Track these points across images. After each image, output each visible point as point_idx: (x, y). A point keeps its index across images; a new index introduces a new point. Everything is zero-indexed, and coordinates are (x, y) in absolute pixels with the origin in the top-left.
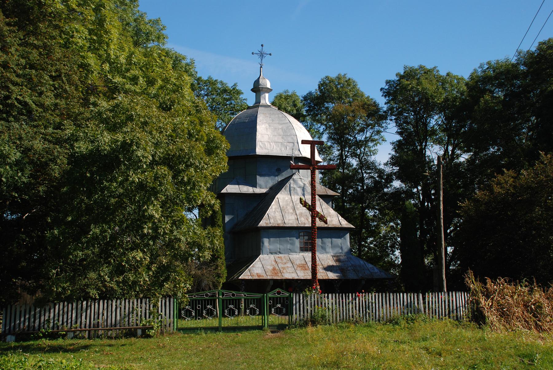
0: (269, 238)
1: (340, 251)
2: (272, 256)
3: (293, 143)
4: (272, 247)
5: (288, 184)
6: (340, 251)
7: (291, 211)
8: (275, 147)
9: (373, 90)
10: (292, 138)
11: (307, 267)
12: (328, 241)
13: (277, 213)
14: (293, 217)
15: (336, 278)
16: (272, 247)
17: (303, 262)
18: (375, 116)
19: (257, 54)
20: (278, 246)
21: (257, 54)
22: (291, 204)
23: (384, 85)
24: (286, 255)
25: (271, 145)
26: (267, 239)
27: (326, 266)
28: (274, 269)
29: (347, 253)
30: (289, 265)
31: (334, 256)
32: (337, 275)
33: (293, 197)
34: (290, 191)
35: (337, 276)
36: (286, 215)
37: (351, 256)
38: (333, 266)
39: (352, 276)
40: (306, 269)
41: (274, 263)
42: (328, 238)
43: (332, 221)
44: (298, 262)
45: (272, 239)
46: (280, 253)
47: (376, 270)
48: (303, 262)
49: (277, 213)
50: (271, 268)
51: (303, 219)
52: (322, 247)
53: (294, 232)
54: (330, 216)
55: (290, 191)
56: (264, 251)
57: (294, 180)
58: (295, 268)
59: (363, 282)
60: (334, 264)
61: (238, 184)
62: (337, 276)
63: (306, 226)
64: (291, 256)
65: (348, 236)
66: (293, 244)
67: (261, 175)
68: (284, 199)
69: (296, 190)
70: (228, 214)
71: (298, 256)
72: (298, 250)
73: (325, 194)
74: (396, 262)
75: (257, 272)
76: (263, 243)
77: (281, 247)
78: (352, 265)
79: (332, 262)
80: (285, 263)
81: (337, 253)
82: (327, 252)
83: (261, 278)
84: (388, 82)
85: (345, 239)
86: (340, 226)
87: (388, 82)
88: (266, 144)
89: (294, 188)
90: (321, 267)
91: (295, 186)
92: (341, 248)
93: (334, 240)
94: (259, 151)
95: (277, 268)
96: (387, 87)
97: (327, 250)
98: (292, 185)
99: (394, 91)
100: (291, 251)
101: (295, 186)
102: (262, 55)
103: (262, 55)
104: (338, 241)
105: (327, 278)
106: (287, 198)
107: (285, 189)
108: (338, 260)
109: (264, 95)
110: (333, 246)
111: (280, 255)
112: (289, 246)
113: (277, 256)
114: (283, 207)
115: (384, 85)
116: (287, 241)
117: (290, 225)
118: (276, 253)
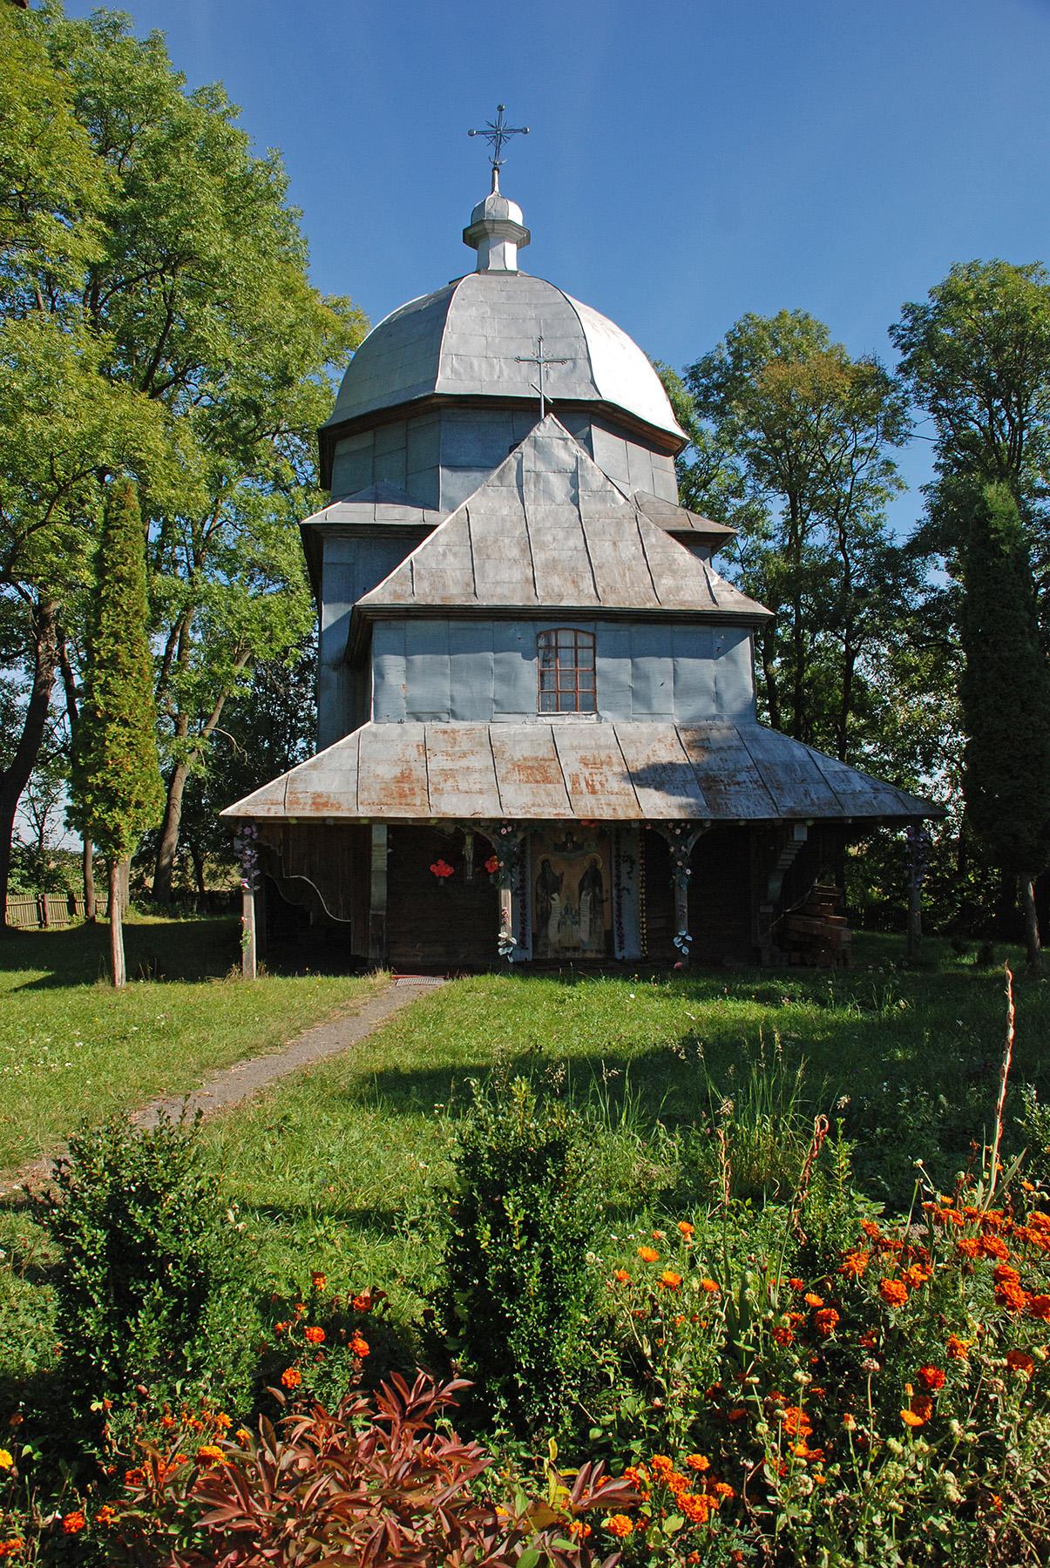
0: (406, 652)
1: (713, 710)
2: (415, 730)
3: (574, 360)
4: (417, 691)
5: (511, 460)
6: (713, 710)
7: (515, 552)
8: (506, 373)
9: (866, 336)
10: (571, 345)
11: (553, 772)
12: (659, 667)
13: (450, 558)
14: (518, 574)
15: (676, 815)
16: (417, 691)
17: (545, 751)
18: (870, 401)
19: (483, 133)
20: (446, 686)
21: (483, 133)
22: (519, 530)
23: (897, 318)
24: (478, 725)
25: (491, 366)
26: (400, 660)
27: (639, 764)
28: (404, 778)
29: (740, 716)
30: (481, 760)
31: (685, 730)
32: (684, 800)
33: (530, 508)
34: (520, 486)
35: (681, 807)
36: (489, 566)
37: (757, 729)
38: (671, 767)
39: (746, 807)
40: (547, 780)
41: (412, 753)
42: (659, 654)
43: (679, 589)
44: (521, 752)
45: (418, 659)
46: (453, 714)
47: (858, 784)
48: (545, 751)
49: (450, 558)
50: (388, 772)
51: (556, 581)
52: (635, 694)
53: (515, 630)
54: (674, 573)
55: (520, 486)
56: (385, 708)
57: (535, 444)
58: (502, 771)
59: (801, 835)
60: (679, 757)
61: (376, 499)
62: (681, 807)
63: (564, 603)
64: (496, 729)
65: (745, 648)
66: (508, 678)
67: (454, 467)
68: (493, 511)
69: (547, 482)
70: (333, 600)
71: (529, 728)
72: (532, 704)
73: (688, 528)
74: (934, 798)
75: (320, 789)
76: (381, 675)
77: (460, 691)
78: (757, 764)
79: (670, 752)
80: (464, 755)
81: (692, 720)
82: (654, 715)
83: (325, 813)
84: (909, 310)
85: (733, 661)
86: (711, 607)
87: (909, 310)
88: (476, 363)
89: (538, 475)
90: (617, 769)
91: (541, 467)
92: (718, 698)
93: (686, 663)
94: (447, 383)
95: (419, 772)
96: (907, 323)
97: (657, 705)
98: (526, 465)
99: (921, 338)
100: (503, 707)
101: (541, 467)
102: (497, 136)
103: (497, 136)
104: (703, 670)
105: (632, 814)
106: (505, 512)
107: (500, 477)
108: (701, 745)
109: (500, 247)
110: (682, 691)
111: (455, 724)
112: (492, 688)
113: (443, 726)
114: (483, 539)
115: (897, 318)
116: (485, 669)
117: (495, 602)
118: (435, 716)
